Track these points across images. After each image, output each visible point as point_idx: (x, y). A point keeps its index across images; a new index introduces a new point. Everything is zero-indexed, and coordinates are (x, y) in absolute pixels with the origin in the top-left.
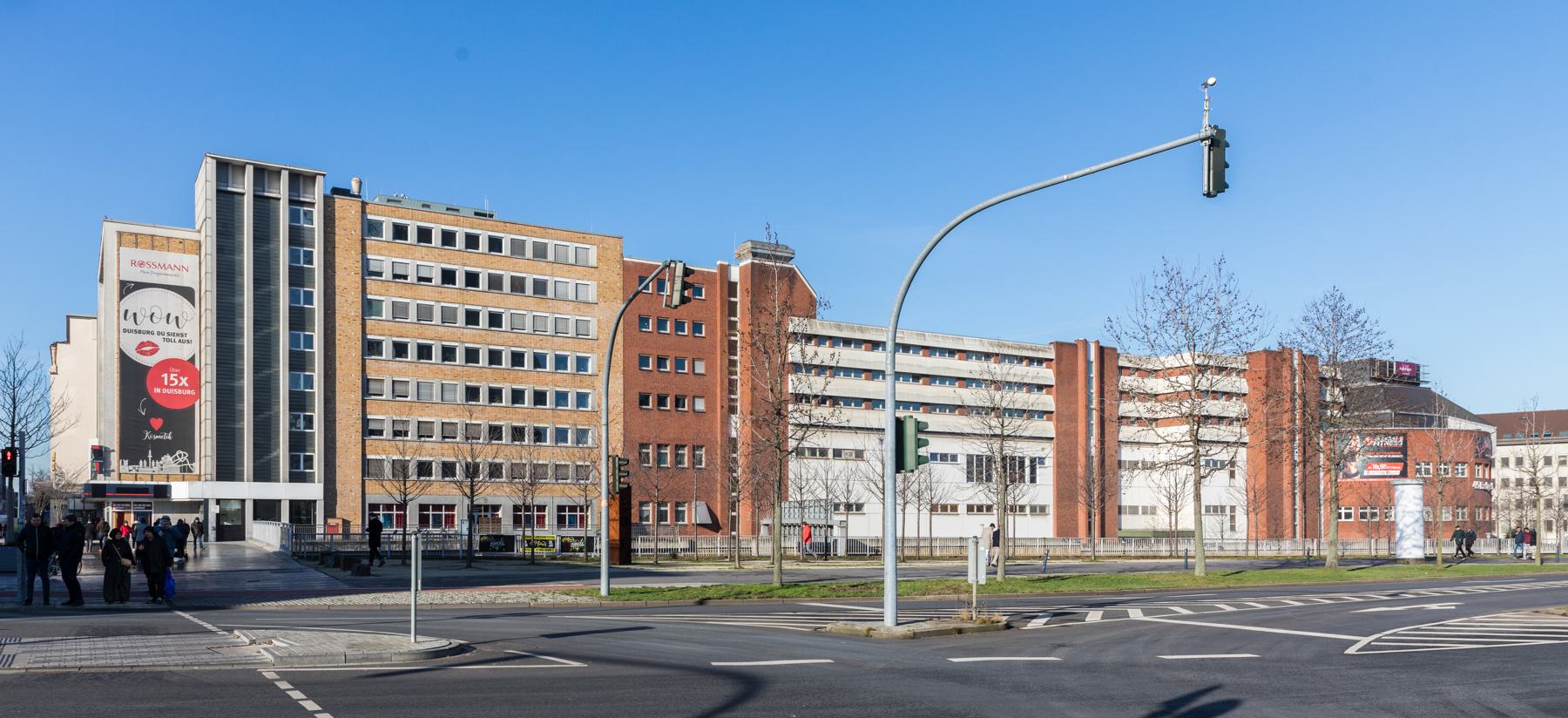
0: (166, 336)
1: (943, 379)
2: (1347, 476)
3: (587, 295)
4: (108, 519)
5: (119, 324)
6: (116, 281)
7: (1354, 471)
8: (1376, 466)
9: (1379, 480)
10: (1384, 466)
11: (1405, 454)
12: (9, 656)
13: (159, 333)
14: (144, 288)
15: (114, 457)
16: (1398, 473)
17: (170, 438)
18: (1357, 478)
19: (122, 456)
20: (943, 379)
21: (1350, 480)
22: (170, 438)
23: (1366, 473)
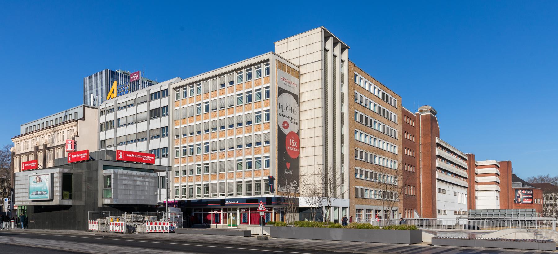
0: (294, 121)
1: (456, 165)
2: (519, 202)
3: (18, 193)
4: (190, 172)
5: (277, 111)
6: (276, 87)
7: (520, 201)
8: (526, 200)
9: (527, 204)
10: (528, 200)
11: (532, 196)
12: (146, 87)
13: (289, 118)
14: (286, 92)
15: (276, 182)
16: (531, 202)
17: (292, 173)
18: (521, 203)
19: (279, 182)
20: (456, 165)
21: (519, 204)
22: (292, 173)
23: (523, 202)
